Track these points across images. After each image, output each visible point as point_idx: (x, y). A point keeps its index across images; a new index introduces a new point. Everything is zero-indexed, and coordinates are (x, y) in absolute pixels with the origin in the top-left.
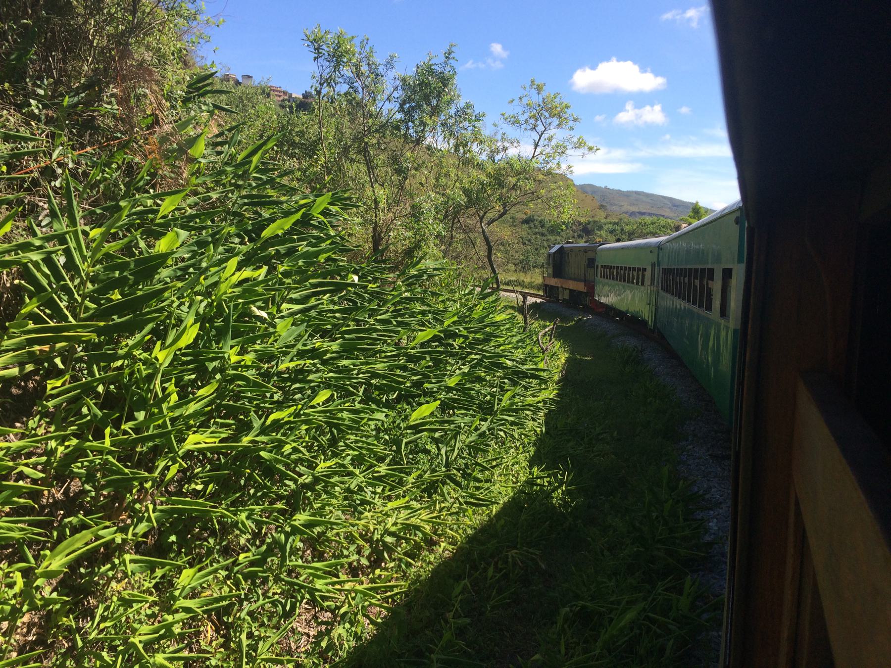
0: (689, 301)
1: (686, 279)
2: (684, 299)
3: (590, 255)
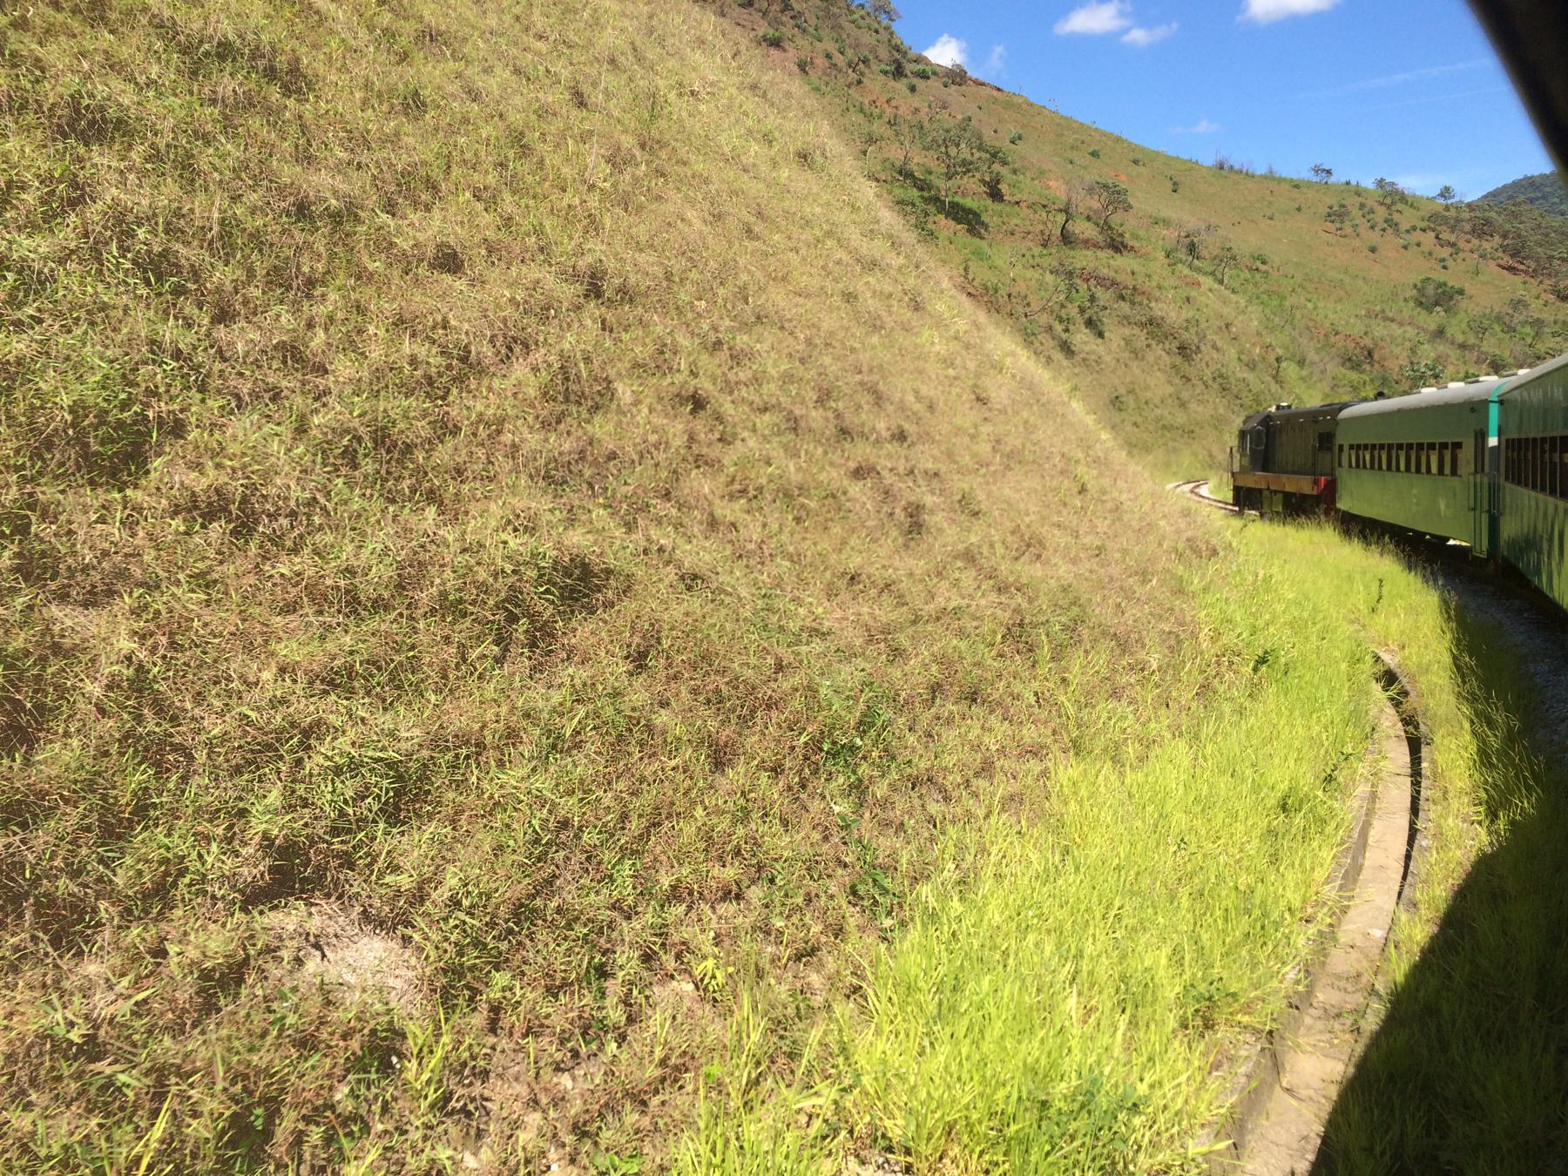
2: (1543, 489)
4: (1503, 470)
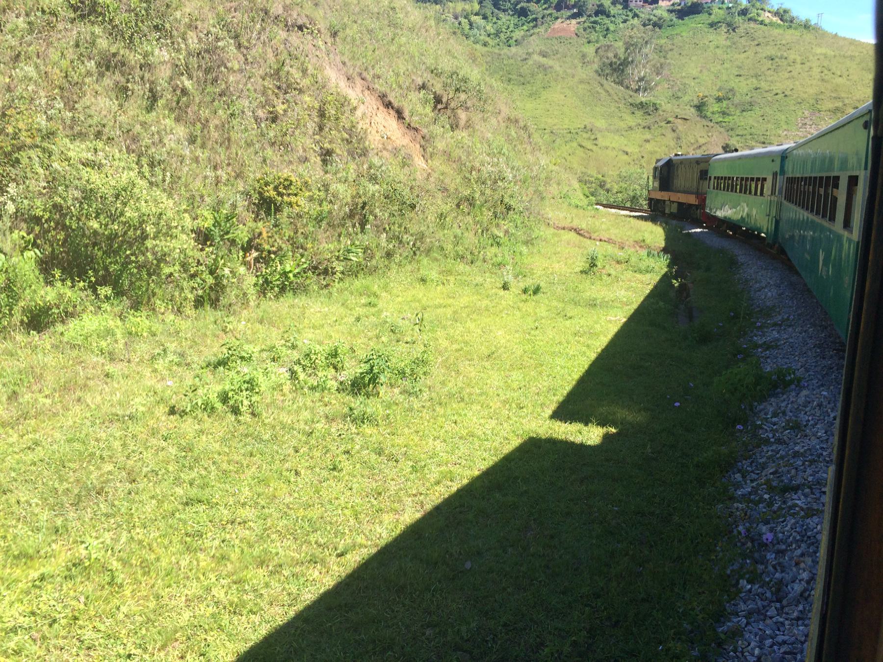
0: (812, 211)
1: (811, 187)
2: (807, 209)
3: (703, 166)
4: (784, 195)
